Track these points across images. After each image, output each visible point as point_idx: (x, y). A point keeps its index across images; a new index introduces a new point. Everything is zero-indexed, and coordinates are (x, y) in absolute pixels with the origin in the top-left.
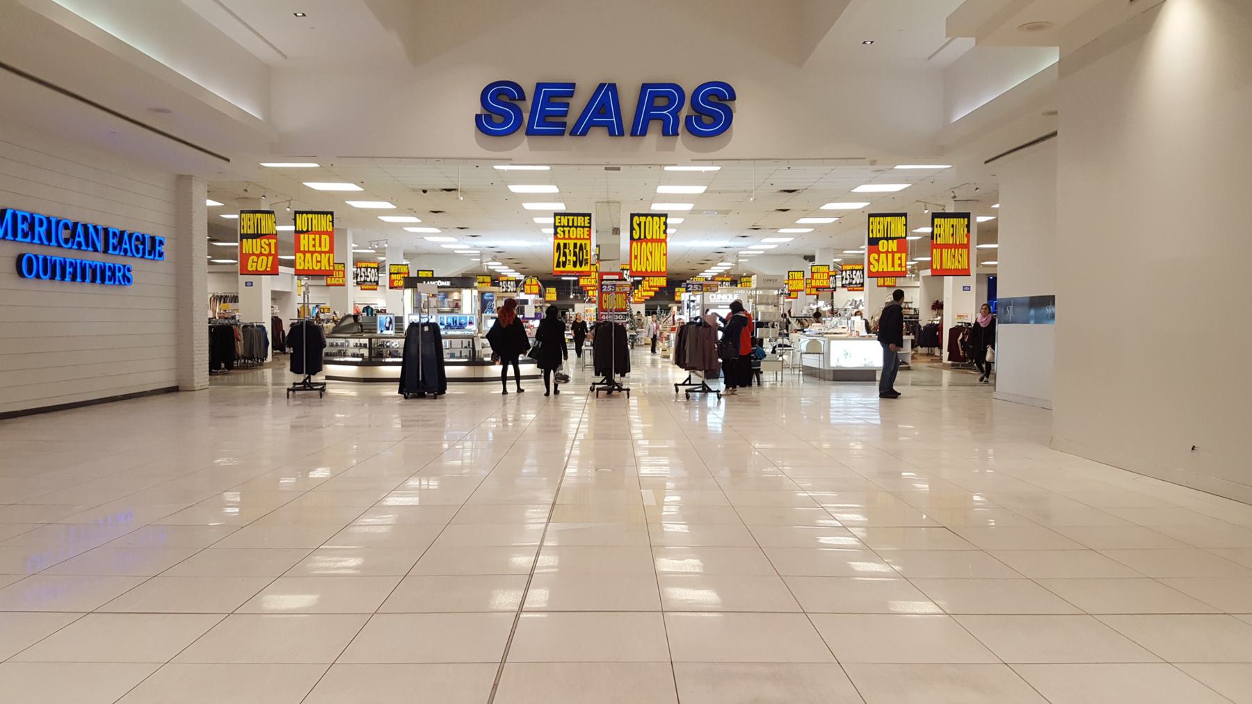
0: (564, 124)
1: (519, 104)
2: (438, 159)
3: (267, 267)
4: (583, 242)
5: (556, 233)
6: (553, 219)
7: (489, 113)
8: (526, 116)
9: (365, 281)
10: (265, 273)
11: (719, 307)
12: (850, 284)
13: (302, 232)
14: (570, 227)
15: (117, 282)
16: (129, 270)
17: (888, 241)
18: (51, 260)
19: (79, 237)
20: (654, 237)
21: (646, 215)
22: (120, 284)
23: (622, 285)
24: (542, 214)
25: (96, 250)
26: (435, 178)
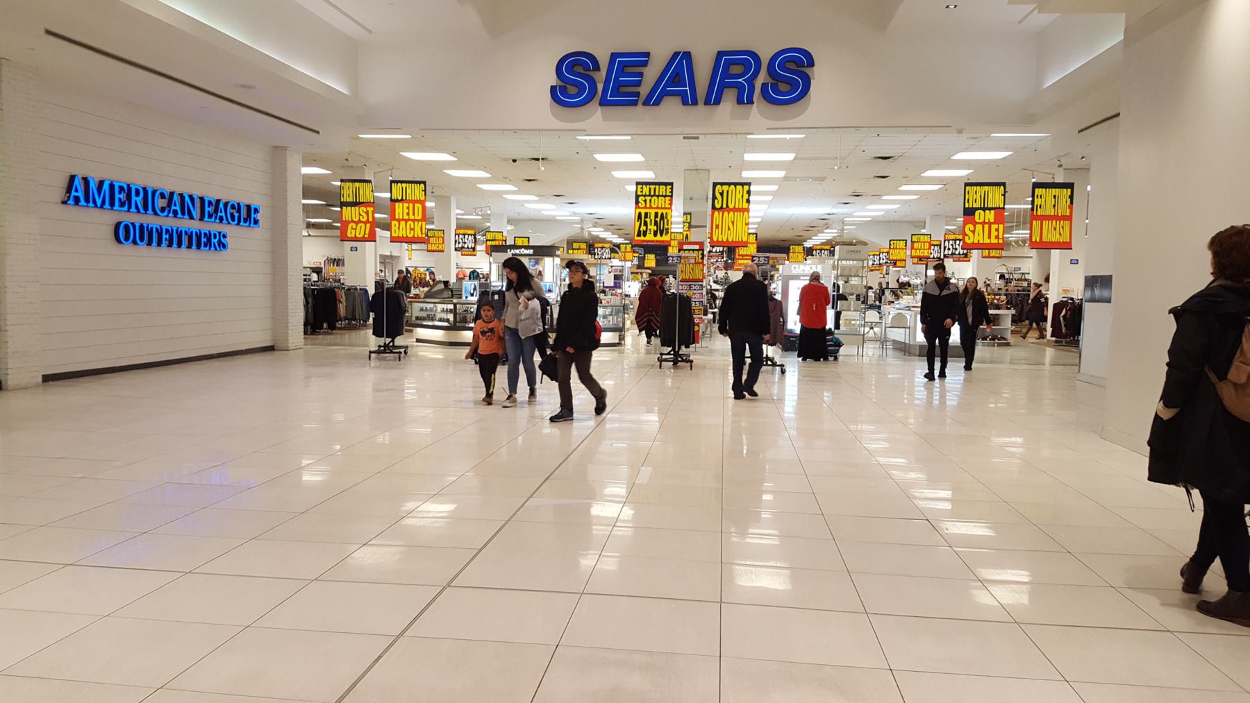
0: (638, 94)
1: (594, 74)
2: (515, 131)
3: (365, 233)
4: (664, 211)
5: (637, 202)
6: (635, 186)
7: (564, 84)
8: (600, 87)
9: (463, 247)
10: (363, 240)
11: (802, 278)
12: (953, 254)
13: (397, 201)
14: (652, 196)
15: (213, 248)
16: (224, 236)
17: (985, 212)
18: (148, 227)
19: (175, 205)
20: (737, 207)
21: (729, 184)
22: (216, 249)
23: (776, 258)
24: (628, 181)
25: (191, 217)
26: (523, 149)
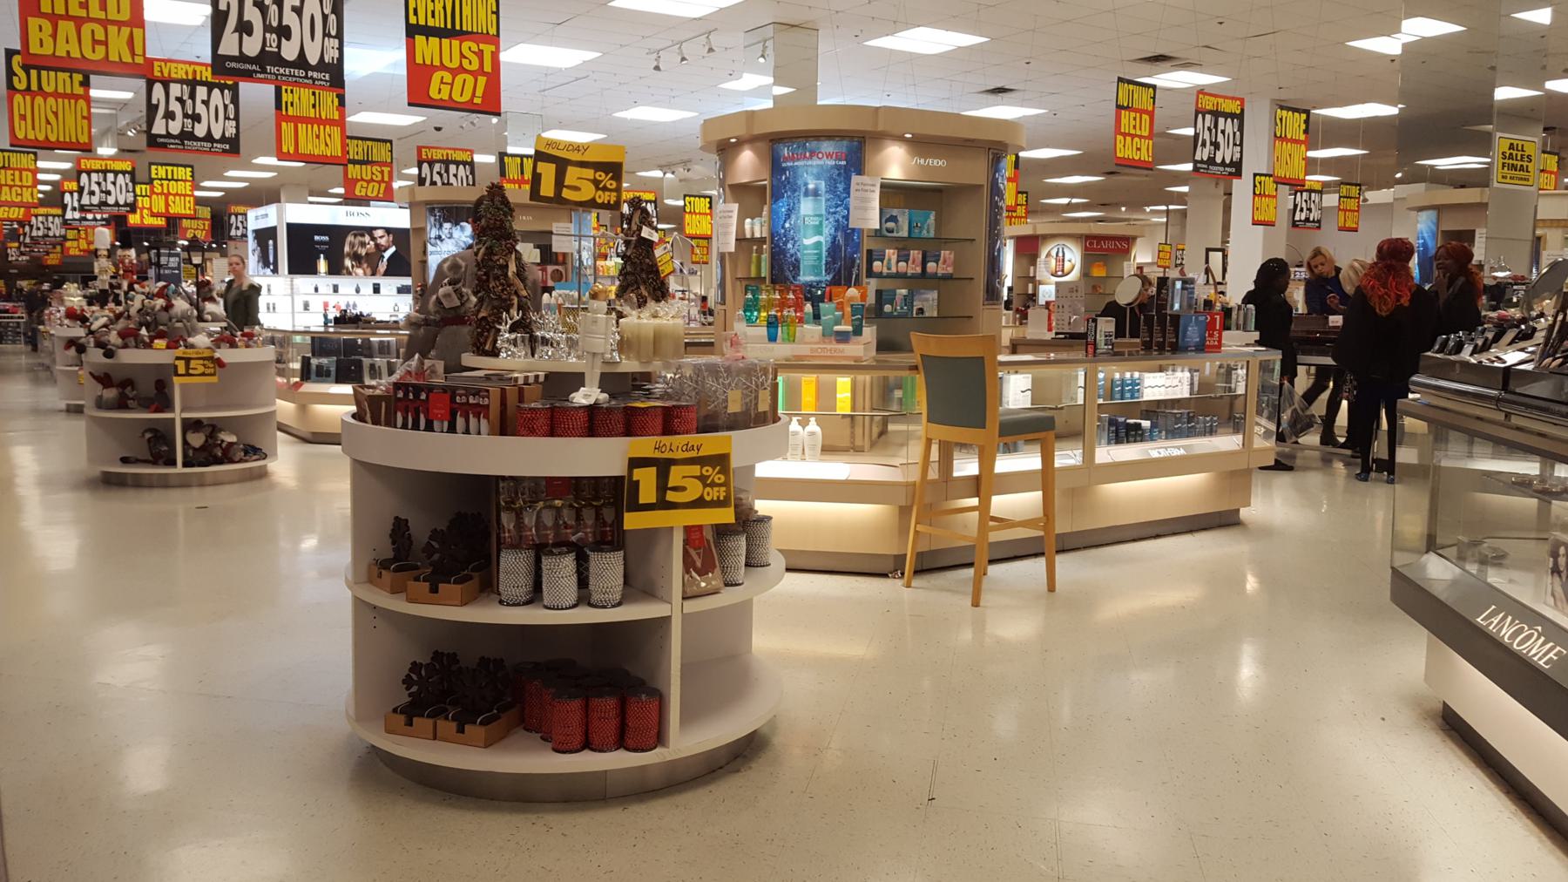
3: (379, 192)
9: (186, 135)
